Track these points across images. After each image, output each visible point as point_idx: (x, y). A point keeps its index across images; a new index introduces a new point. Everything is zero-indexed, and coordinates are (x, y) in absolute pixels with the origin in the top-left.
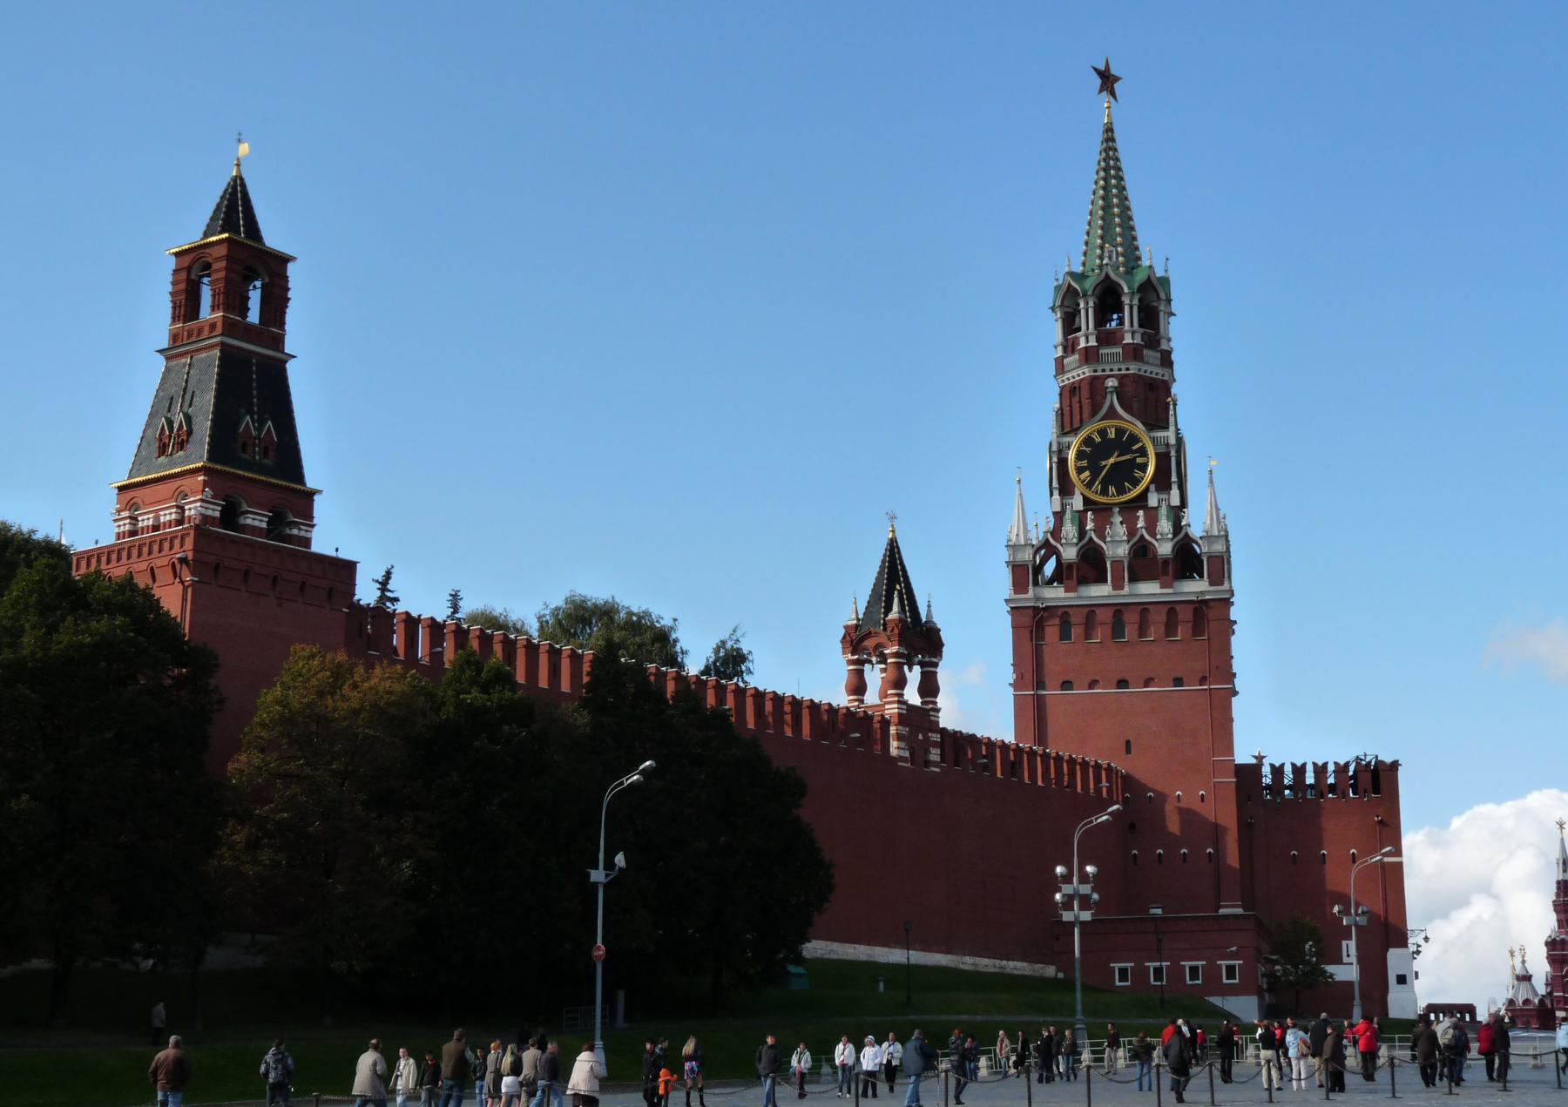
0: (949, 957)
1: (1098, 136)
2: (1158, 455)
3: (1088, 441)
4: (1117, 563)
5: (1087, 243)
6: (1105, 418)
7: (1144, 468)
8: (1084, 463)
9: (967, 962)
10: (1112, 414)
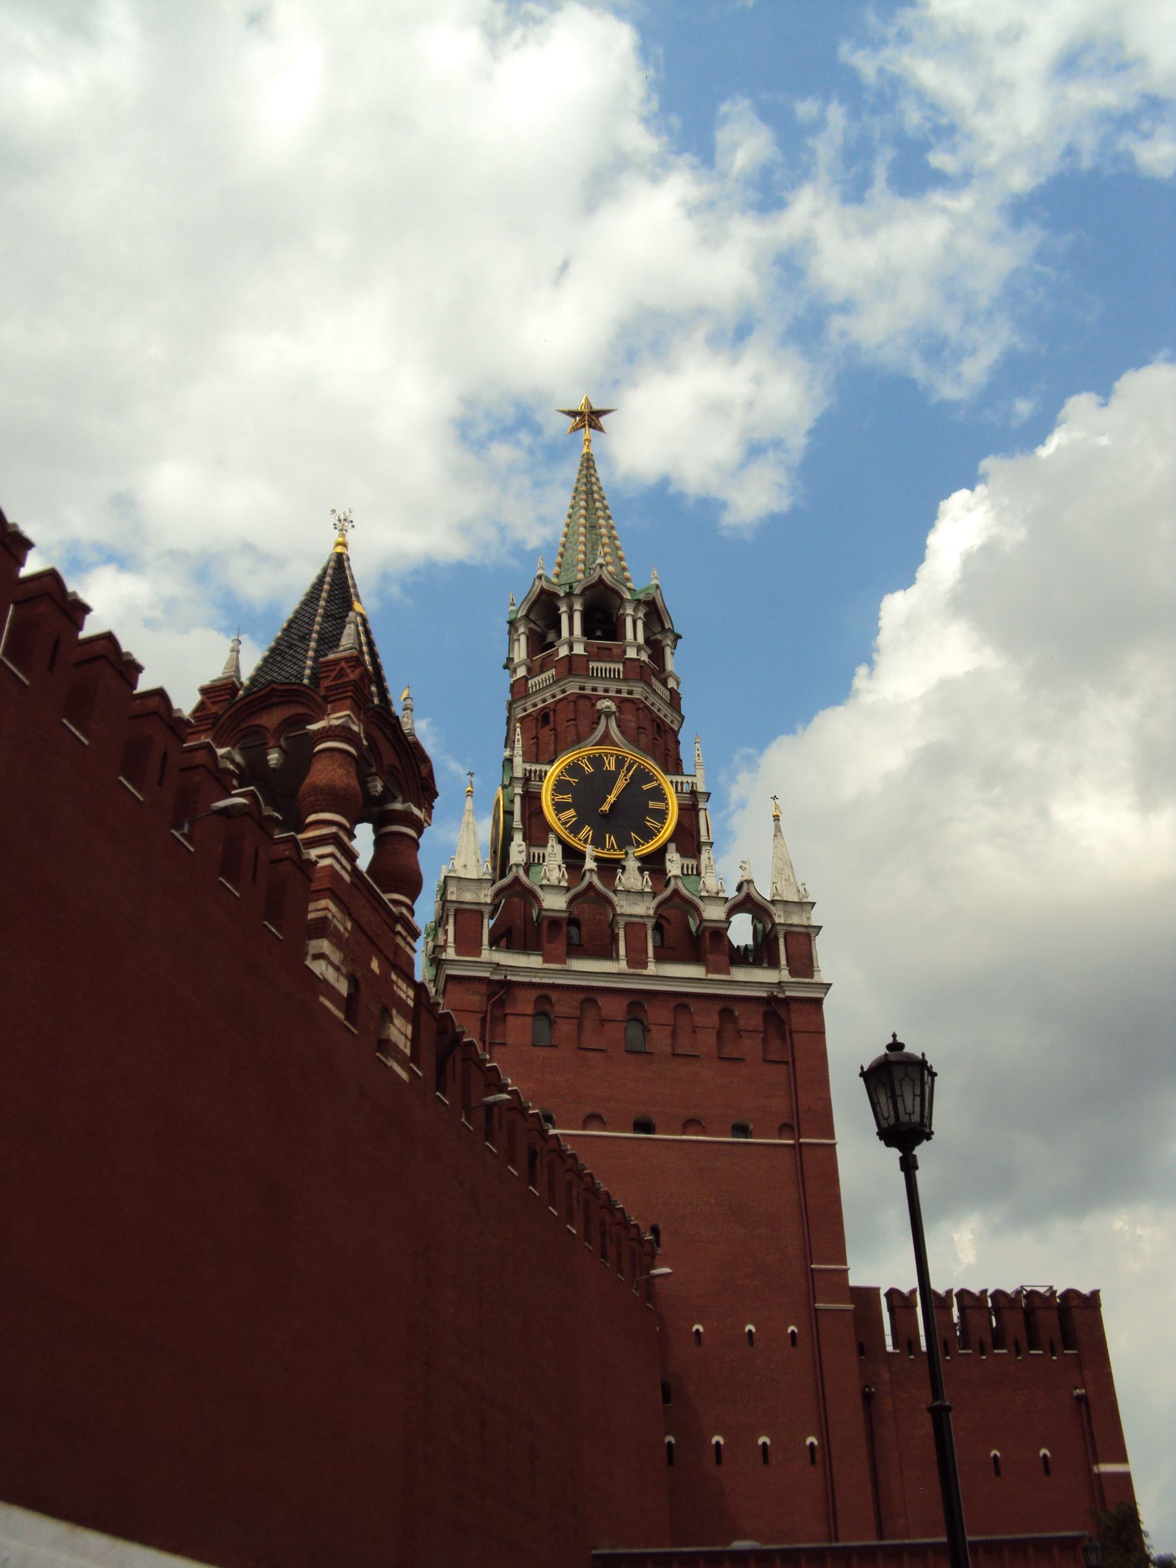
0: (620, 735)
1: (493, 805)
2: (681, 808)
3: (573, 769)
4: (635, 927)
5: (570, 516)
6: (600, 743)
7: (661, 816)
8: (568, 798)
9: (21, 676)
10: (606, 739)
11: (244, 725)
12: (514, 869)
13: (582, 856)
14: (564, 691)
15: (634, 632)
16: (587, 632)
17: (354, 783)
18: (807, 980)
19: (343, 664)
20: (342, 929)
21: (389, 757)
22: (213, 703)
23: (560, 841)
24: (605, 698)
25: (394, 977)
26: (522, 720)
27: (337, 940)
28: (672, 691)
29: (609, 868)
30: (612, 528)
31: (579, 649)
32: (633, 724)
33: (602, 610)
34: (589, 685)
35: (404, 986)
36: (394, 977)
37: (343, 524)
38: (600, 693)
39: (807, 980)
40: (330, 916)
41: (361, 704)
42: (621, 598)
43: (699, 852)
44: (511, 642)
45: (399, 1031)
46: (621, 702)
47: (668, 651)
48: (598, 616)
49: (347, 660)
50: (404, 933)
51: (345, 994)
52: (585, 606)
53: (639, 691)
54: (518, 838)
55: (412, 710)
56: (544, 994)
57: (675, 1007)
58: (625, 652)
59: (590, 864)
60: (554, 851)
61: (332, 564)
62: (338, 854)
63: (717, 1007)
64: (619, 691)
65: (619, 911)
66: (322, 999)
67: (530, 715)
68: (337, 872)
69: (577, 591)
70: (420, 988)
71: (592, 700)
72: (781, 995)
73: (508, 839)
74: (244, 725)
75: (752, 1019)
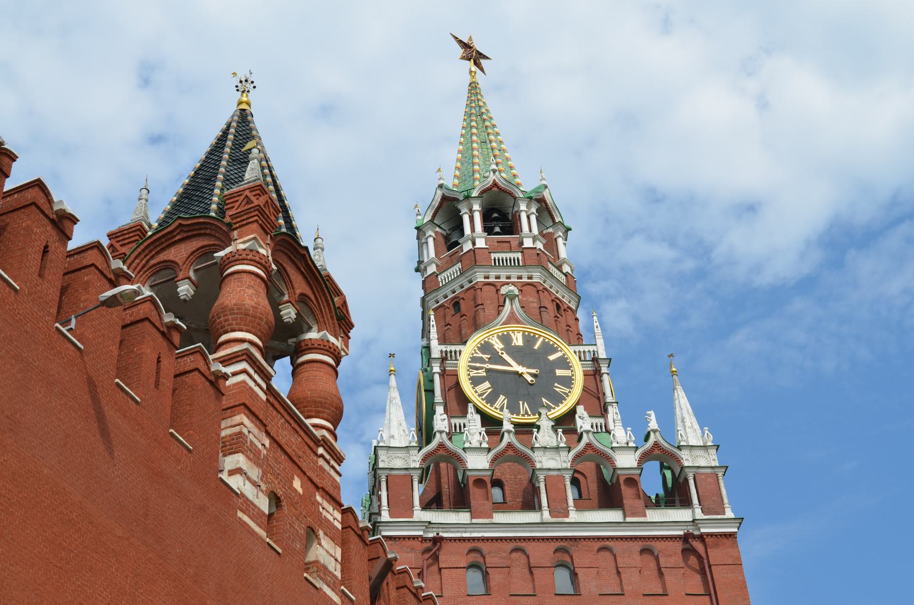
4: (555, 482)
7: (568, 382)
10: (512, 319)
11: (153, 262)
12: (438, 435)
13: (500, 423)
14: (470, 282)
15: (529, 224)
16: (488, 230)
17: (264, 302)
18: (719, 517)
19: (247, 193)
20: (260, 447)
21: (301, 286)
22: (121, 246)
23: (478, 411)
24: (507, 284)
25: (319, 498)
26: (435, 310)
27: (254, 456)
28: (566, 275)
29: (525, 429)
30: (501, 142)
31: (481, 243)
32: (535, 305)
33: (500, 215)
34: (493, 274)
35: (330, 509)
36: (319, 498)
37: (245, 85)
38: (503, 280)
39: (719, 517)
40: (245, 431)
41: (267, 228)
42: (515, 198)
43: (606, 411)
44: (421, 246)
45: (326, 552)
46: (522, 287)
47: (560, 241)
48: (495, 215)
49: (251, 189)
50: (328, 457)
51: (267, 512)
52: (482, 206)
53: (537, 277)
54: (440, 409)
55: (323, 249)
56: (475, 546)
57: (599, 550)
58: (522, 243)
59: (507, 426)
60: (474, 422)
61: (236, 118)
62: (251, 371)
63: (637, 546)
64: (520, 278)
65: (538, 466)
66: (240, 514)
67: (442, 306)
68: (250, 388)
69: (475, 194)
70: (348, 512)
71: (496, 287)
72: (696, 533)
73: (431, 412)
74: (153, 262)
75: (672, 556)
